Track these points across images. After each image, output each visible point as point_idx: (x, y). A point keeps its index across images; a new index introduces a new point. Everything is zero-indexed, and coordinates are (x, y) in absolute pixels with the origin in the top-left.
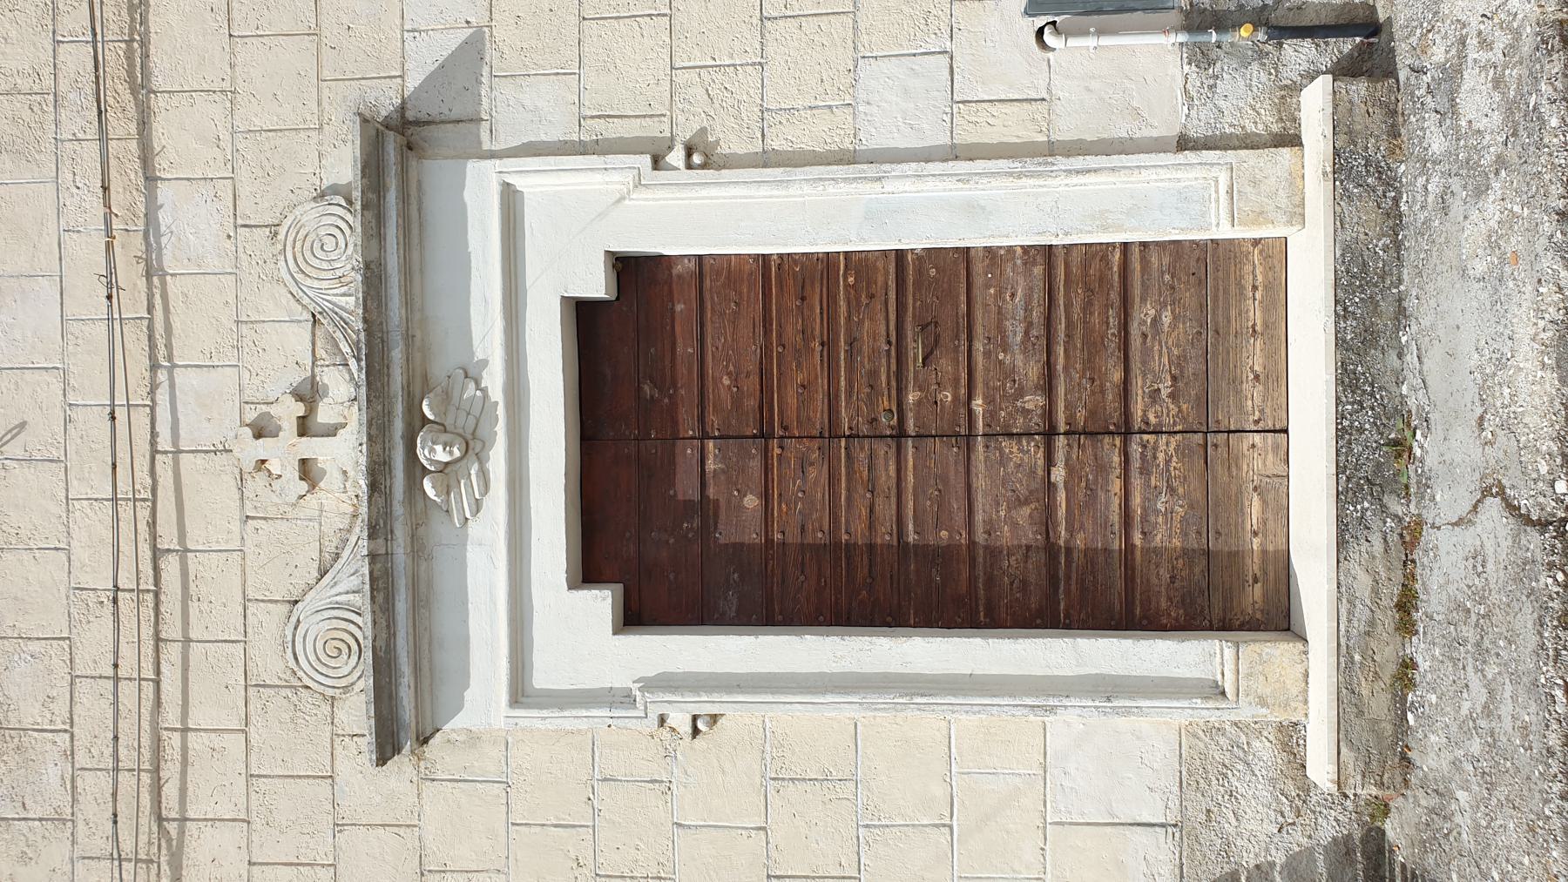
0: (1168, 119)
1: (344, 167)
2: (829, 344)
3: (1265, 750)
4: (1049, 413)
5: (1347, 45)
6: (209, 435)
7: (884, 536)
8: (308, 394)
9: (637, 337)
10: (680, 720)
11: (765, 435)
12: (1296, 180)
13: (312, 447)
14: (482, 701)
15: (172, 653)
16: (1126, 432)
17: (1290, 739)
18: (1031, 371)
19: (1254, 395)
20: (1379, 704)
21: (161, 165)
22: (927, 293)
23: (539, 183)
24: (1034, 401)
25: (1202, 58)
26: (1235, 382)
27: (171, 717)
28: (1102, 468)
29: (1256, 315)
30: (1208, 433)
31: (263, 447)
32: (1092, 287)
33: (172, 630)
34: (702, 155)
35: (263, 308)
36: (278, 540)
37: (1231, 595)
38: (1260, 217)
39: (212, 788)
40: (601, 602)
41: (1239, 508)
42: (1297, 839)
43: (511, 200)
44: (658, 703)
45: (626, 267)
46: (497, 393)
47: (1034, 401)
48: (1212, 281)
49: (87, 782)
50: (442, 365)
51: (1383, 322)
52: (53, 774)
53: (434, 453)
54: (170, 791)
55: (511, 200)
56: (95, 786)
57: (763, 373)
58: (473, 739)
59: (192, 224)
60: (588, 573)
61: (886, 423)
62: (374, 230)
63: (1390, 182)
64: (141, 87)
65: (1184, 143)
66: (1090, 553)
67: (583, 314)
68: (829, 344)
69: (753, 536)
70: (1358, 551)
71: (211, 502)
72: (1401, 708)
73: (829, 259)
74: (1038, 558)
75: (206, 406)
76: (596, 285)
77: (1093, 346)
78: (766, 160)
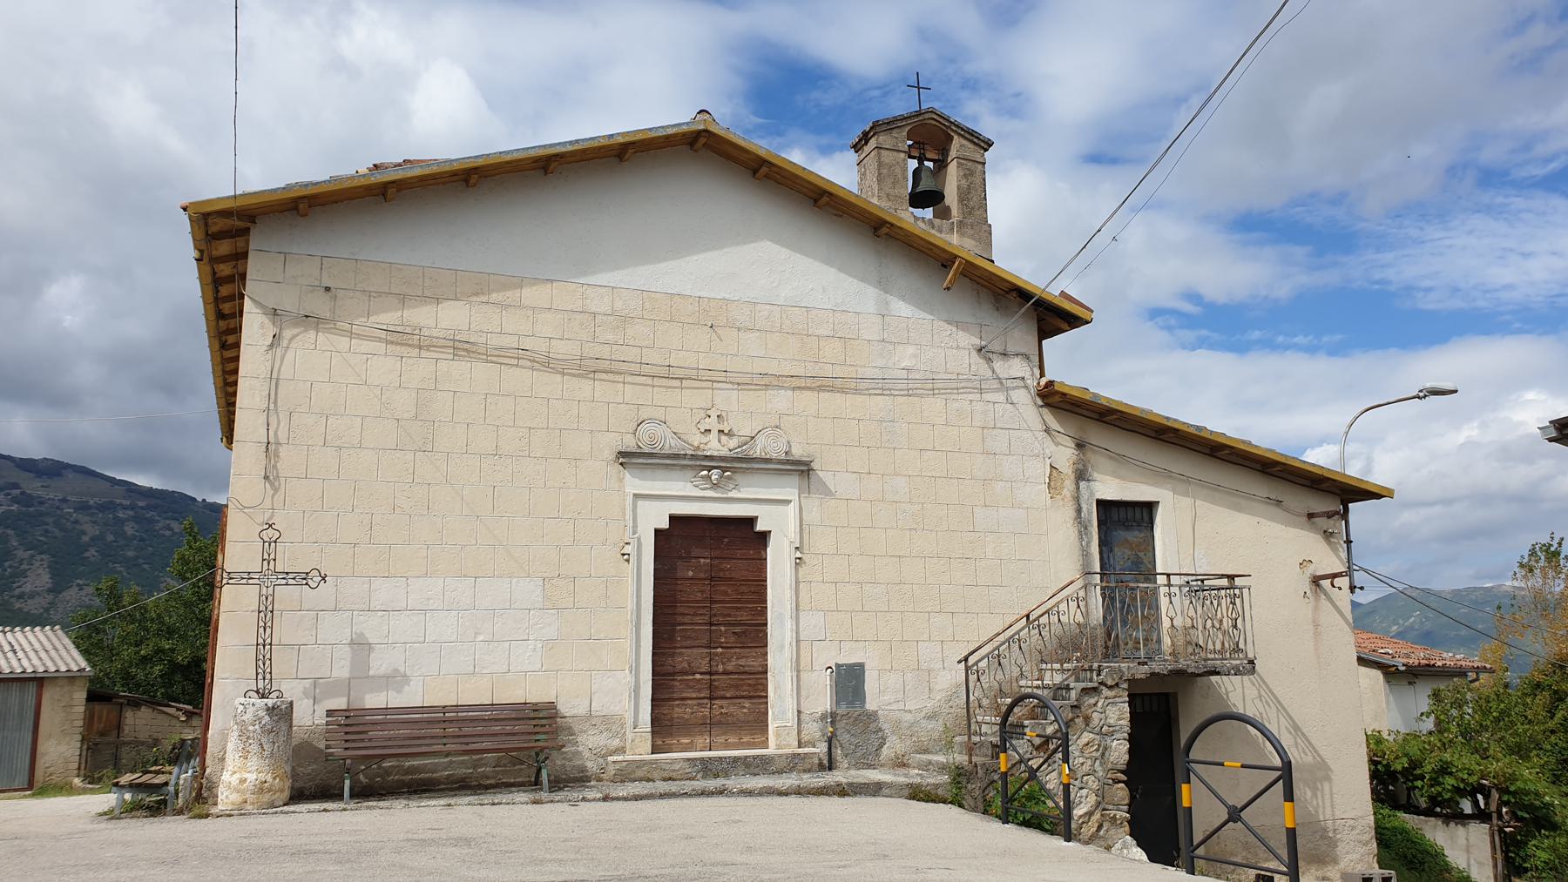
0: (806, 711)
1: (798, 452)
2: (739, 601)
3: (616, 743)
4: (717, 673)
5: (826, 762)
6: (718, 400)
7: (680, 619)
8: (730, 434)
9: (744, 537)
10: (627, 549)
11: (712, 579)
12: (789, 746)
13: (714, 433)
14: (634, 483)
15: (649, 380)
16: (710, 699)
17: (622, 750)
18: (730, 667)
19: (721, 739)
20: (640, 773)
21: (797, 392)
22: (754, 634)
23: (792, 510)
24: (721, 668)
25: (823, 717)
26: (725, 733)
27: (629, 379)
28: (699, 691)
29: (745, 740)
30: (710, 725)
31: (714, 417)
32: (754, 686)
33: (657, 381)
34: (799, 562)
35: (756, 420)
36: (682, 420)
37: (663, 728)
38: (778, 735)
39: (603, 390)
40: (664, 524)
41: (688, 735)
42: (587, 754)
43: (788, 502)
44: (634, 543)
45: (764, 536)
46: (730, 495)
47: (721, 668)
48: (759, 723)
49: (607, 348)
50: (739, 478)
51: (752, 770)
52: (610, 337)
53: (715, 474)
54: (604, 376)
55: (788, 502)
56: (605, 352)
57: (731, 579)
58: (621, 480)
59: (781, 400)
60: (672, 518)
61: (714, 620)
62: (780, 462)
63: (791, 770)
64: (820, 389)
65: (799, 712)
66: (672, 687)
67: (751, 521)
68: (739, 601)
69: (679, 574)
70: (686, 765)
71: (696, 398)
72: (641, 780)
73: (765, 601)
74: (671, 670)
75: (726, 399)
76: (760, 527)
77: (737, 687)
78: (797, 582)
